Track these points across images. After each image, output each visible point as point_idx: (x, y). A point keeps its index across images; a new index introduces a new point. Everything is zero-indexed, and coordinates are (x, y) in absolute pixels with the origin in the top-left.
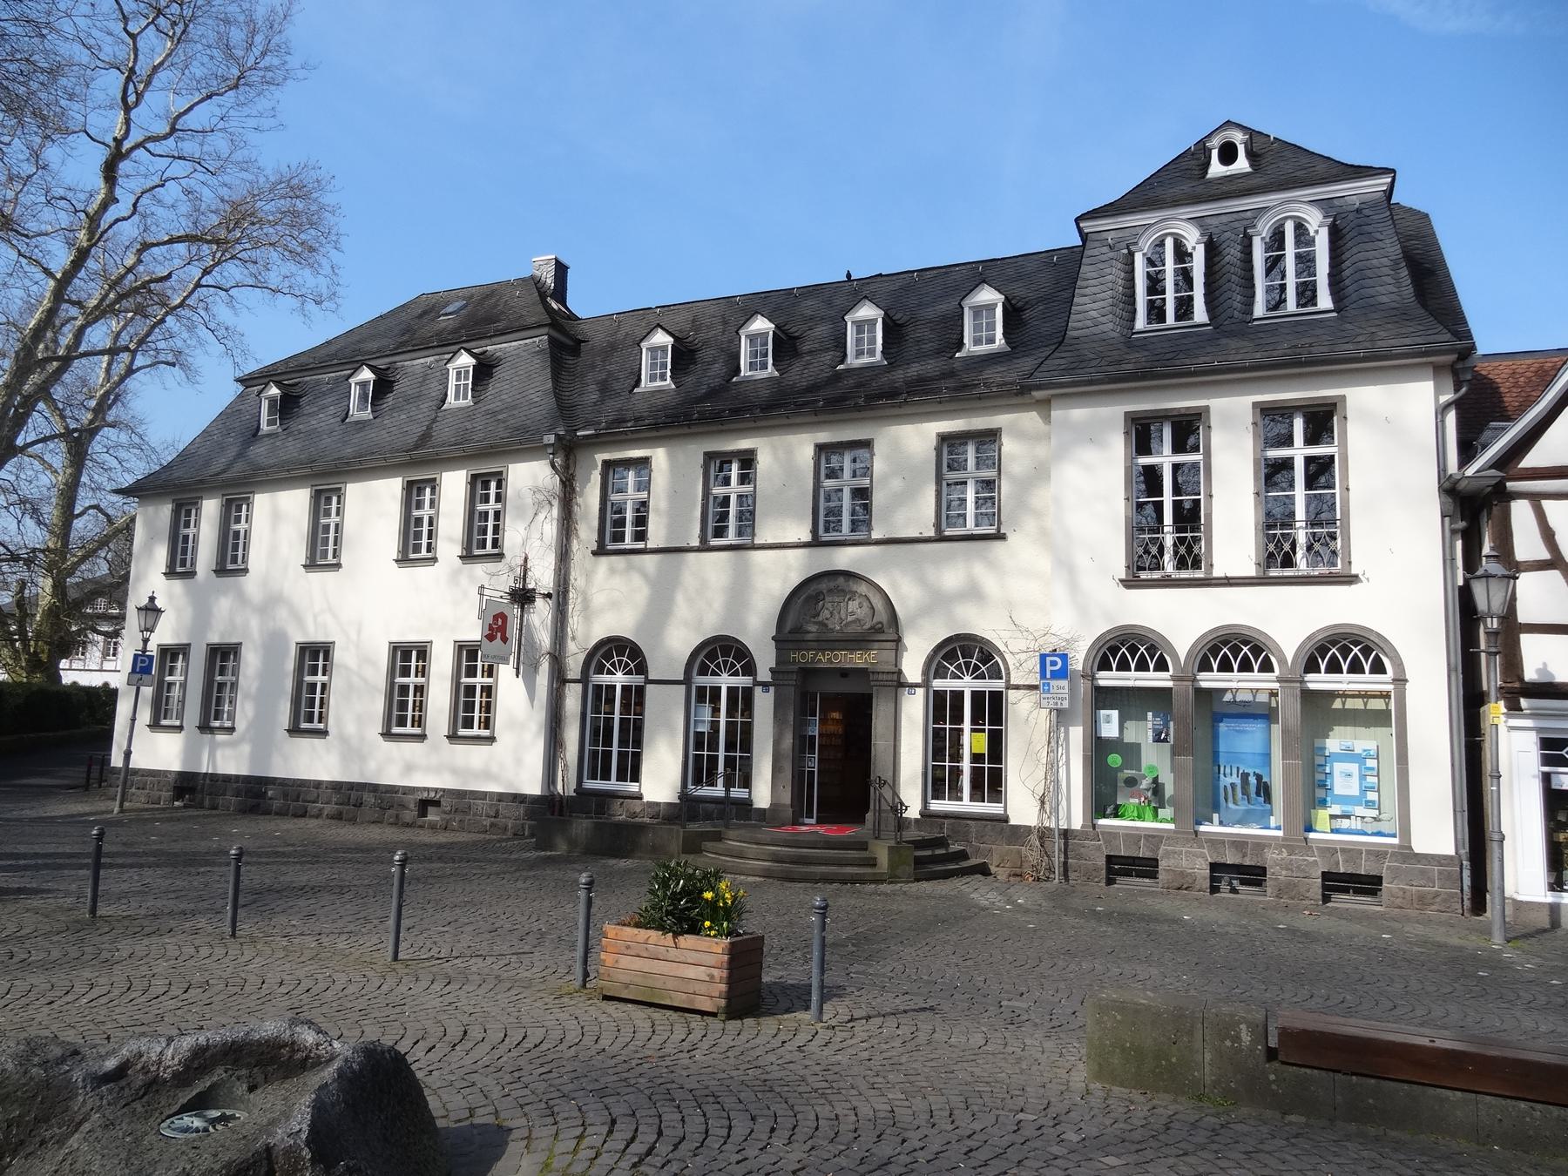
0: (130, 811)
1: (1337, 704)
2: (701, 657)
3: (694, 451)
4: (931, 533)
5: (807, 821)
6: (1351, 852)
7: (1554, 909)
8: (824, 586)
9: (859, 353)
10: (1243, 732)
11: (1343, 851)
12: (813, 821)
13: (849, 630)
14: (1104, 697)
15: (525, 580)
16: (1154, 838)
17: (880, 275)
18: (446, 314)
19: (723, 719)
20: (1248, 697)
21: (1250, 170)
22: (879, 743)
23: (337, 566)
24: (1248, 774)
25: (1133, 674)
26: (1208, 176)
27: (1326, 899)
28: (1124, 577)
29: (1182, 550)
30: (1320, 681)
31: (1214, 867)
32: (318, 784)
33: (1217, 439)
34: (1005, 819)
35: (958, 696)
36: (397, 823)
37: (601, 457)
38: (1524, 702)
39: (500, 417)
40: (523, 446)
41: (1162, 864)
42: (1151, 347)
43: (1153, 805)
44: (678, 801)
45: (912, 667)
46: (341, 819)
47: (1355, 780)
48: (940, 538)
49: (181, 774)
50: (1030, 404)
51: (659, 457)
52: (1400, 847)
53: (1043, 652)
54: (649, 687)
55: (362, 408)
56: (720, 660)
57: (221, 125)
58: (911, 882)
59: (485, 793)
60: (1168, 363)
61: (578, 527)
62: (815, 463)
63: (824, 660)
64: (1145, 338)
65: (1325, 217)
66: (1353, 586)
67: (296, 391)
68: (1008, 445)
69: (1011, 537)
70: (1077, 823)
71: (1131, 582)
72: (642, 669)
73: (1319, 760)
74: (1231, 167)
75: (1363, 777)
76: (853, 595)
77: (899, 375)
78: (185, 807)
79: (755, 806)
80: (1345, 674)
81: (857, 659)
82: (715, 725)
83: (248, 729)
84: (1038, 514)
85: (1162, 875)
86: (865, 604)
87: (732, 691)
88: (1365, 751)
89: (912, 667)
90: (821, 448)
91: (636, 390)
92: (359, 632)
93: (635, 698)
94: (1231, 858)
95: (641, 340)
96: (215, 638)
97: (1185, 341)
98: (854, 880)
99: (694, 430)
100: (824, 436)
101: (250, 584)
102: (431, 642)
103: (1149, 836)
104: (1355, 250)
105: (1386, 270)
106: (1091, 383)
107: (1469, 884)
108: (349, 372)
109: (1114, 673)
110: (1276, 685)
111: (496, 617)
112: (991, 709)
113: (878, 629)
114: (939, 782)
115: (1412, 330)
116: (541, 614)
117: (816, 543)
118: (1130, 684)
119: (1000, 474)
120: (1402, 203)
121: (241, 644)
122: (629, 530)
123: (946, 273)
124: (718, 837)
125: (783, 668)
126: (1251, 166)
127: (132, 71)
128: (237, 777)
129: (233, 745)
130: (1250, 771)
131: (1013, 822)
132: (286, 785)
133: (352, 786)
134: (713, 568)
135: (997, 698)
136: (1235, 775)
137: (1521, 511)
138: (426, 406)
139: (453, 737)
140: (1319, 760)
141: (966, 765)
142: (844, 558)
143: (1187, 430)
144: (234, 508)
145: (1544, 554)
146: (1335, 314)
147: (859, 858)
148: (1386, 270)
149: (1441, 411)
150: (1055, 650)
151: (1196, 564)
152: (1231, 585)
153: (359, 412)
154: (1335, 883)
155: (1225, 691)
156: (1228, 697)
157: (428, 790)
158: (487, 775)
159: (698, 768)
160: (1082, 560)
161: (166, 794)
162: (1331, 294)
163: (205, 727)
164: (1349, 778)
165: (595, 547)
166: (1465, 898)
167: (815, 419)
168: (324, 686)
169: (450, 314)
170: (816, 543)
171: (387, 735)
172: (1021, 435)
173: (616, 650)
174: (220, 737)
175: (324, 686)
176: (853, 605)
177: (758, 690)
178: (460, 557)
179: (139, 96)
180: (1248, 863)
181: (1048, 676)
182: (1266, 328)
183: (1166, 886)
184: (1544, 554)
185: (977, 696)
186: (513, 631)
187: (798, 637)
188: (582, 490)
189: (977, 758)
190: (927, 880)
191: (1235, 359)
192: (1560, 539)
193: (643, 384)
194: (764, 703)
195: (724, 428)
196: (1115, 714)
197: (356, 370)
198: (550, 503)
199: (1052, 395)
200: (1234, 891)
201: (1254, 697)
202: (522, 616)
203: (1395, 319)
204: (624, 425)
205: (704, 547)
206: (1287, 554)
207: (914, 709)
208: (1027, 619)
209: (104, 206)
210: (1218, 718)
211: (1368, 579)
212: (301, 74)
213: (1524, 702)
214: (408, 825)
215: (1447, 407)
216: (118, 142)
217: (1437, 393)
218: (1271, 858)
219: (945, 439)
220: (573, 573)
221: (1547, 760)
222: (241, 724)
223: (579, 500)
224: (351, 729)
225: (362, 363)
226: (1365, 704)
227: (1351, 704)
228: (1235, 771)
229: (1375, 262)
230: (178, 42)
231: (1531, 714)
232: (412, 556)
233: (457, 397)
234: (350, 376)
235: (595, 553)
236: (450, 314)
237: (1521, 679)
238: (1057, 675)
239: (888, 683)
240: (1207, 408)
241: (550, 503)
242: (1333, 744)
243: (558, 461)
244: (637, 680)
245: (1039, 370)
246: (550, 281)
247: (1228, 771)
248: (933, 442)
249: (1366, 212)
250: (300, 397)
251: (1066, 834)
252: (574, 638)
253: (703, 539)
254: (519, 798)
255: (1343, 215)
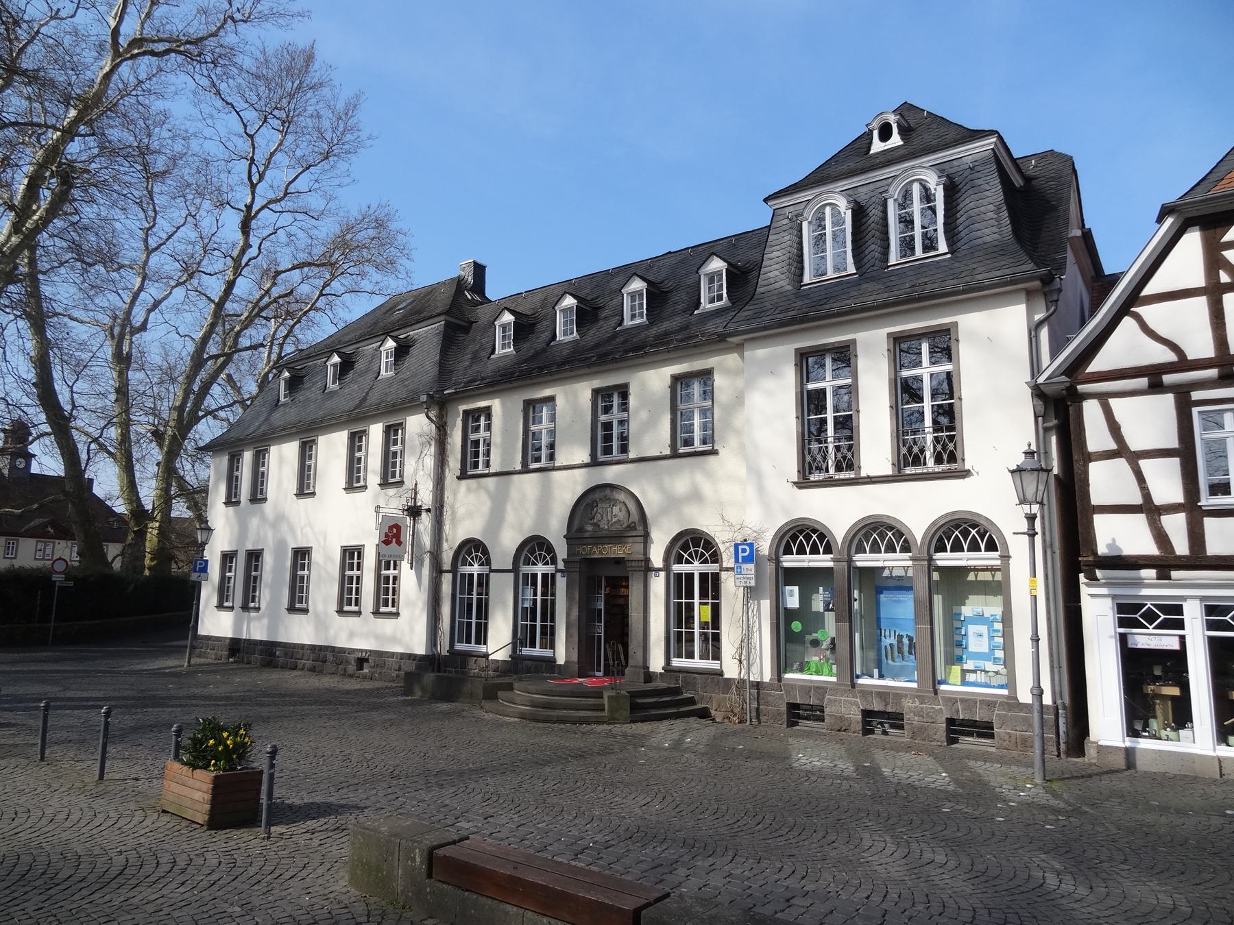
0: (195, 665)
1: (971, 577)
2: (677, 548)
3: (517, 400)
4: (667, 452)
5: (597, 674)
6: (969, 701)
7: (1129, 753)
8: (597, 496)
9: (633, 317)
10: (900, 601)
11: (962, 700)
12: (601, 674)
13: (613, 529)
14: (791, 576)
15: (415, 499)
16: (821, 689)
17: (670, 253)
18: (399, 310)
19: (539, 598)
20: (902, 573)
21: (902, 143)
22: (635, 615)
23: (313, 494)
24: (902, 636)
25: (808, 557)
26: (871, 152)
27: (952, 740)
28: (796, 480)
29: (939, 448)
30: (946, 559)
31: (867, 713)
32: (303, 646)
33: (862, 364)
34: (721, 673)
35: (690, 576)
36: (345, 674)
37: (463, 407)
38: (1099, 573)
39: (406, 383)
40: (409, 405)
41: (827, 710)
42: (811, 296)
43: (831, 661)
44: (510, 659)
45: (657, 557)
46: (315, 671)
47: (985, 639)
48: (675, 455)
49: (232, 639)
50: (732, 348)
51: (496, 405)
52: (1008, 697)
53: (737, 542)
54: (492, 575)
55: (334, 382)
56: (692, 550)
57: (316, 185)
58: (627, 723)
59: (393, 654)
60: (820, 308)
61: (449, 459)
62: (592, 403)
63: (598, 553)
64: (810, 288)
65: (939, 177)
66: (966, 479)
67: (301, 373)
68: (719, 380)
69: (721, 451)
70: (767, 677)
71: (804, 482)
72: (488, 562)
73: (957, 624)
74: (887, 143)
75: (991, 638)
76: (615, 502)
77: (654, 331)
78: (235, 662)
79: (558, 663)
80: (966, 553)
81: (617, 551)
82: (535, 601)
83: (267, 608)
84: (738, 432)
85: (827, 719)
86: (624, 508)
87: (545, 576)
88: (992, 616)
89: (657, 557)
90: (596, 392)
91: (492, 356)
92: (325, 540)
93: (484, 581)
94: (877, 706)
95: (495, 320)
96: (250, 547)
97: (836, 289)
98: (587, 721)
99: (514, 385)
100: (598, 383)
101: (268, 507)
102: (311, 548)
103: (817, 687)
104: (967, 201)
105: (991, 215)
106: (765, 328)
107: (1065, 730)
108: (325, 359)
109: (795, 557)
110: (910, 563)
111: (391, 528)
112: (711, 586)
113: (632, 527)
114: (678, 642)
115: (1004, 263)
116: (426, 521)
117: (594, 463)
118: (805, 565)
119: (713, 404)
120: (1056, 150)
121: (263, 550)
122: (544, 453)
123: (713, 246)
124: (510, 687)
125: (572, 559)
126: (902, 139)
127: (252, 160)
128: (261, 641)
129: (259, 619)
130: (904, 633)
131: (726, 676)
132: (286, 647)
133: (321, 648)
134: (528, 484)
135: (716, 577)
136: (893, 637)
137: (1091, 411)
138: (371, 376)
139: (376, 613)
140: (957, 624)
141: (697, 630)
142: (611, 474)
143: (844, 356)
144: (260, 457)
145: (1112, 445)
146: (949, 256)
147: (595, 705)
148: (991, 215)
149: (1034, 330)
150: (745, 540)
151: (850, 467)
152: (874, 483)
153: (332, 386)
154: (957, 728)
155: (883, 568)
156: (886, 573)
157: (361, 651)
158: (394, 639)
159: (523, 636)
160: (766, 467)
161: (225, 653)
162: (946, 240)
163: (245, 608)
164: (980, 638)
165: (458, 474)
166: (1061, 741)
167: (588, 371)
168: (358, 578)
169: (401, 309)
170: (594, 463)
171: (340, 612)
172: (727, 372)
173: (473, 548)
174: (253, 614)
175: (358, 578)
176: (616, 510)
177: (558, 575)
178: (380, 485)
179: (261, 177)
180: (889, 710)
181: (740, 561)
182: (897, 272)
183: (830, 728)
184: (1112, 445)
185: (703, 576)
186: (407, 537)
187: (580, 535)
188: (451, 434)
189: (704, 625)
190: (642, 721)
191: (869, 300)
192: (1125, 431)
193: (497, 352)
194: (561, 583)
195: (534, 381)
196: (796, 589)
197: (329, 357)
198: (429, 443)
199: (745, 340)
200: (885, 733)
201: (906, 572)
202: (414, 526)
203: (993, 255)
204: (474, 384)
205: (525, 470)
206: (952, 452)
207: (658, 585)
208: (733, 515)
209: (243, 251)
210: (880, 590)
211: (978, 473)
212: (368, 143)
213: (1099, 573)
214: (351, 676)
215: (1040, 324)
216: (249, 207)
217: (1030, 314)
218: (908, 705)
219: (676, 379)
220: (446, 493)
221: (1122, 623)
222: (263, 606)
223: (449, 440)
224: (320, 607)
225: (333, 351)
226: (993, 576)
227: (983, 576)
228: (892, 634)
229: (982, 209)
230: (286, 134)
231: (1105, 583)
232: (355, 485)
233: (386, 371)
234: (326, 361)
235: (459, 478)
236: (401, 309)
237: (1095, 553)
238: (747, 560)
239: (637, 569)
240: (854, 341)
241: (429, 443)
242: (967, 611)
243: (432, 414)
244: (485, 569)
245: (733, 321)
246: (470, 280)
247: (887, 633)
248: (668, 381)
249: (978, 168)
250: (304, 376)
251: (758, 685)
252: (447, 540)
253: (524, 463)
254: (411, 657)
255: (960, 173)
